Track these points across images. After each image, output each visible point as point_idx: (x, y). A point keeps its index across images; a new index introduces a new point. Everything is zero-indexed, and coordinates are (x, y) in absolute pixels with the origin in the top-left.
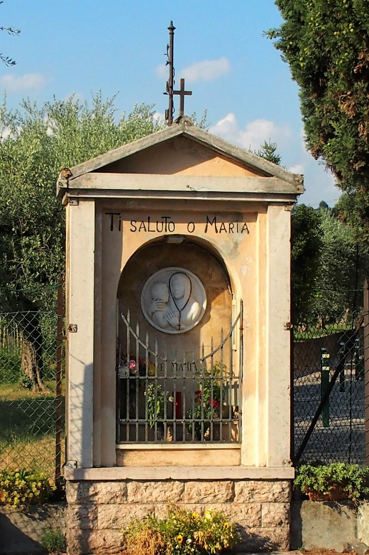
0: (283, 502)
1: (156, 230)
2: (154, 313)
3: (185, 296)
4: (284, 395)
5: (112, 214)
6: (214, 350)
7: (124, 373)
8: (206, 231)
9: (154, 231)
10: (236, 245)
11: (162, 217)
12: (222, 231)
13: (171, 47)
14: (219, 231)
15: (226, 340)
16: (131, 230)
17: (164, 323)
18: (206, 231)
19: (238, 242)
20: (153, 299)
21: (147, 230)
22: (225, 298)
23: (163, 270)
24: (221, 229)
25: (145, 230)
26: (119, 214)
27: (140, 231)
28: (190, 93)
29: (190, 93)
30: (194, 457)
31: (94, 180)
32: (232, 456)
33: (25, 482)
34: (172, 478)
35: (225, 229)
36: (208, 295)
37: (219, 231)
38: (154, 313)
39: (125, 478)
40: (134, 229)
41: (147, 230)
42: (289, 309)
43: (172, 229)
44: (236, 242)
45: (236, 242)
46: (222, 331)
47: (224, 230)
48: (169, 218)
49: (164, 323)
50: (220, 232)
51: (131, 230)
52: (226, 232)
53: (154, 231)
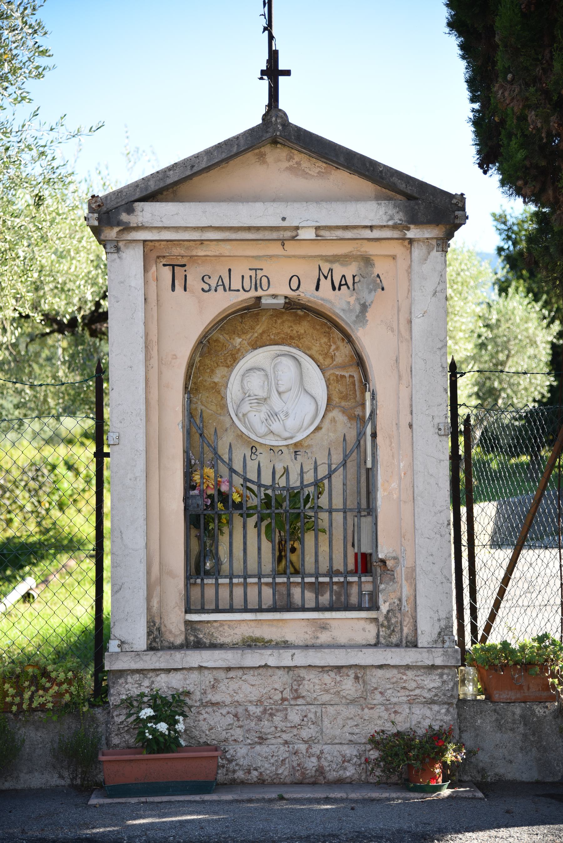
0: (445, 703)
1: (241, 289)
2: (246, 414)
3: (239, 378)
4: (441, 536)
5: (173, 266)
6: (333, 469)
7: (196, 505)
8: (317, 288)
9: (238, 290)
10: (364, 308)
11: (250, 269)
12: (342, 287)
13: (268, 28)
14: (337, 286)
15: (352, 452)
16: (203, 290)
17: (262, 430)
18: (317, 288)
19: (367, 304)
20: (246, 394)
21: (227, 288)
22: (355, 391)
23: (261, 350)
24: (340, 285)
25: (225, 290)
26: (184, 266)
27: (216, 290)
28: (287, 73)
29: (287, 73)
30: (306, 633)
31: (141, 214)
32: (364, 630)
33: (479, 402)
34: (269, 664)
35: (346, 284)
36: (330, 386)
37: (337, 286)
38: (246, 414)
39: (196, 666)
40: (206, 287)
41: (227, 288)
42: (428, 182)
43: (265, 288)
44: (365, 303)
45: (365, 303)
46: (344, 439)
47: (346, 286)
48: (262, 269)
49: (262, 430)
50: (339, 289)
51: (203, 290)
52: (348, 288)
53: (238, 290)
